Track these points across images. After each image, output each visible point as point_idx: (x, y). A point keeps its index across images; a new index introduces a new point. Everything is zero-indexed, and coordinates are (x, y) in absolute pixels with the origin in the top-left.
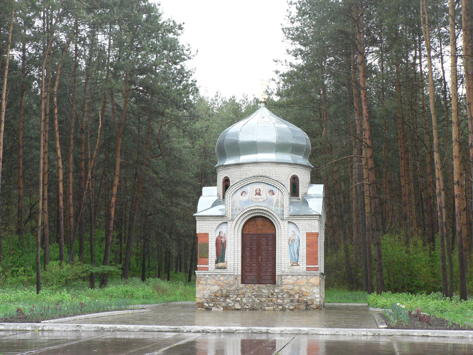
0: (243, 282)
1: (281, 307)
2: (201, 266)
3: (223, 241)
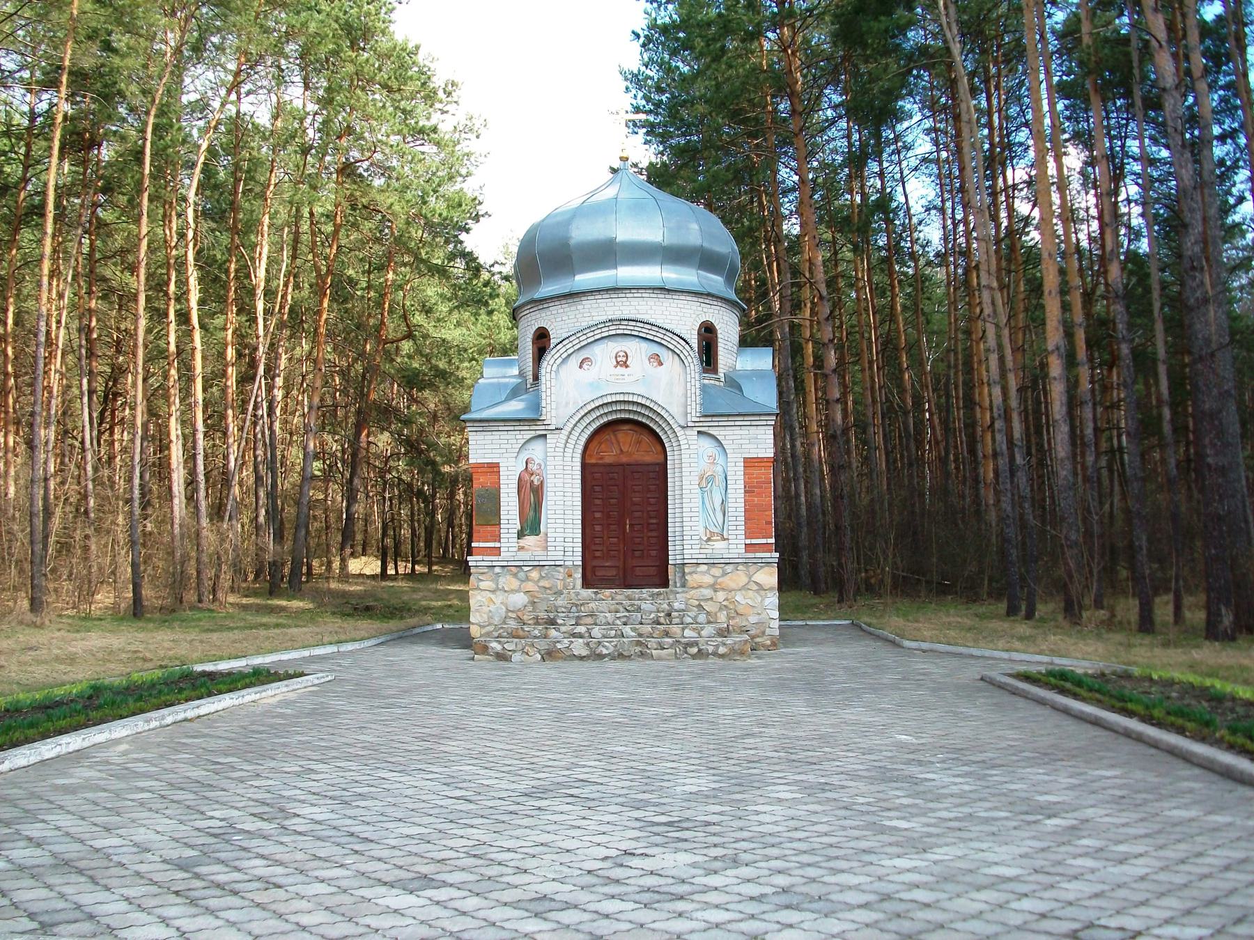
0: (586, 584)
1: (695, 650)
2: (482, 545)
3: (536, 483)
